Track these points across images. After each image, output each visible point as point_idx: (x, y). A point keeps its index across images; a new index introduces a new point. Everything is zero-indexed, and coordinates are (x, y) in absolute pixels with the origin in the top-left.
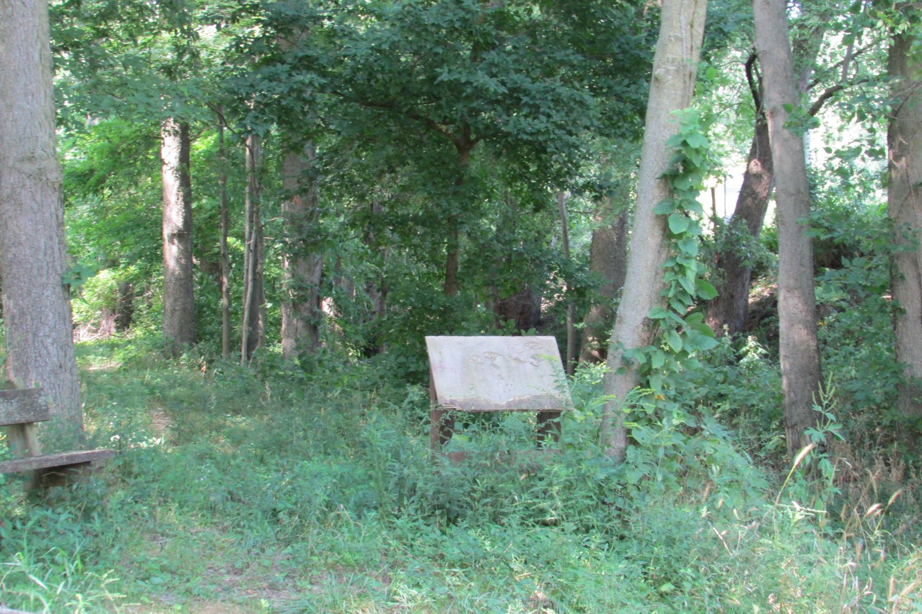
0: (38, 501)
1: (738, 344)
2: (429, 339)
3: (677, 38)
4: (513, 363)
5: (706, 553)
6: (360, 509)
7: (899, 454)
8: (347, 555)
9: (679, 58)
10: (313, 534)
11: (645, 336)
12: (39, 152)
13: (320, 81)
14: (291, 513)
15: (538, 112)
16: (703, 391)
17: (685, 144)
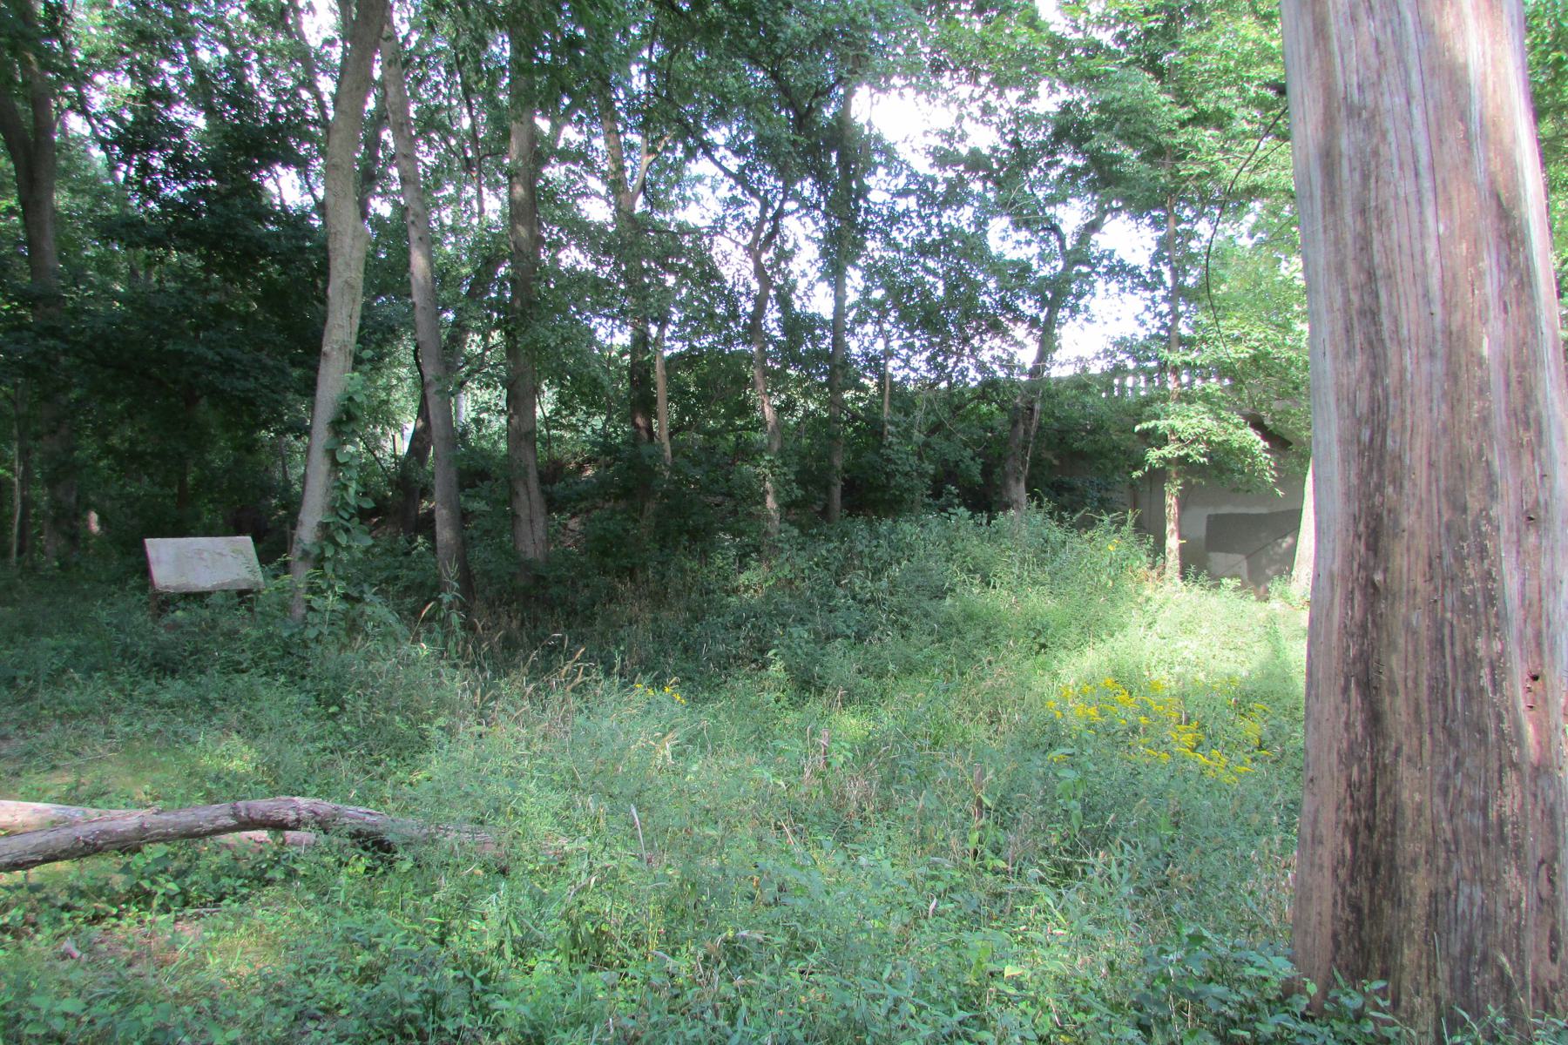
0: (175, 688)
1: (411, 541)
2: (148, 541)
5: (362, 685)
6: (89, 672)
7: (517, 611)
8: (74, 707)
10: (43, 695)
13: (61, 346)
14: (27, 679)
16: (385, 574)
17: (351, 399)
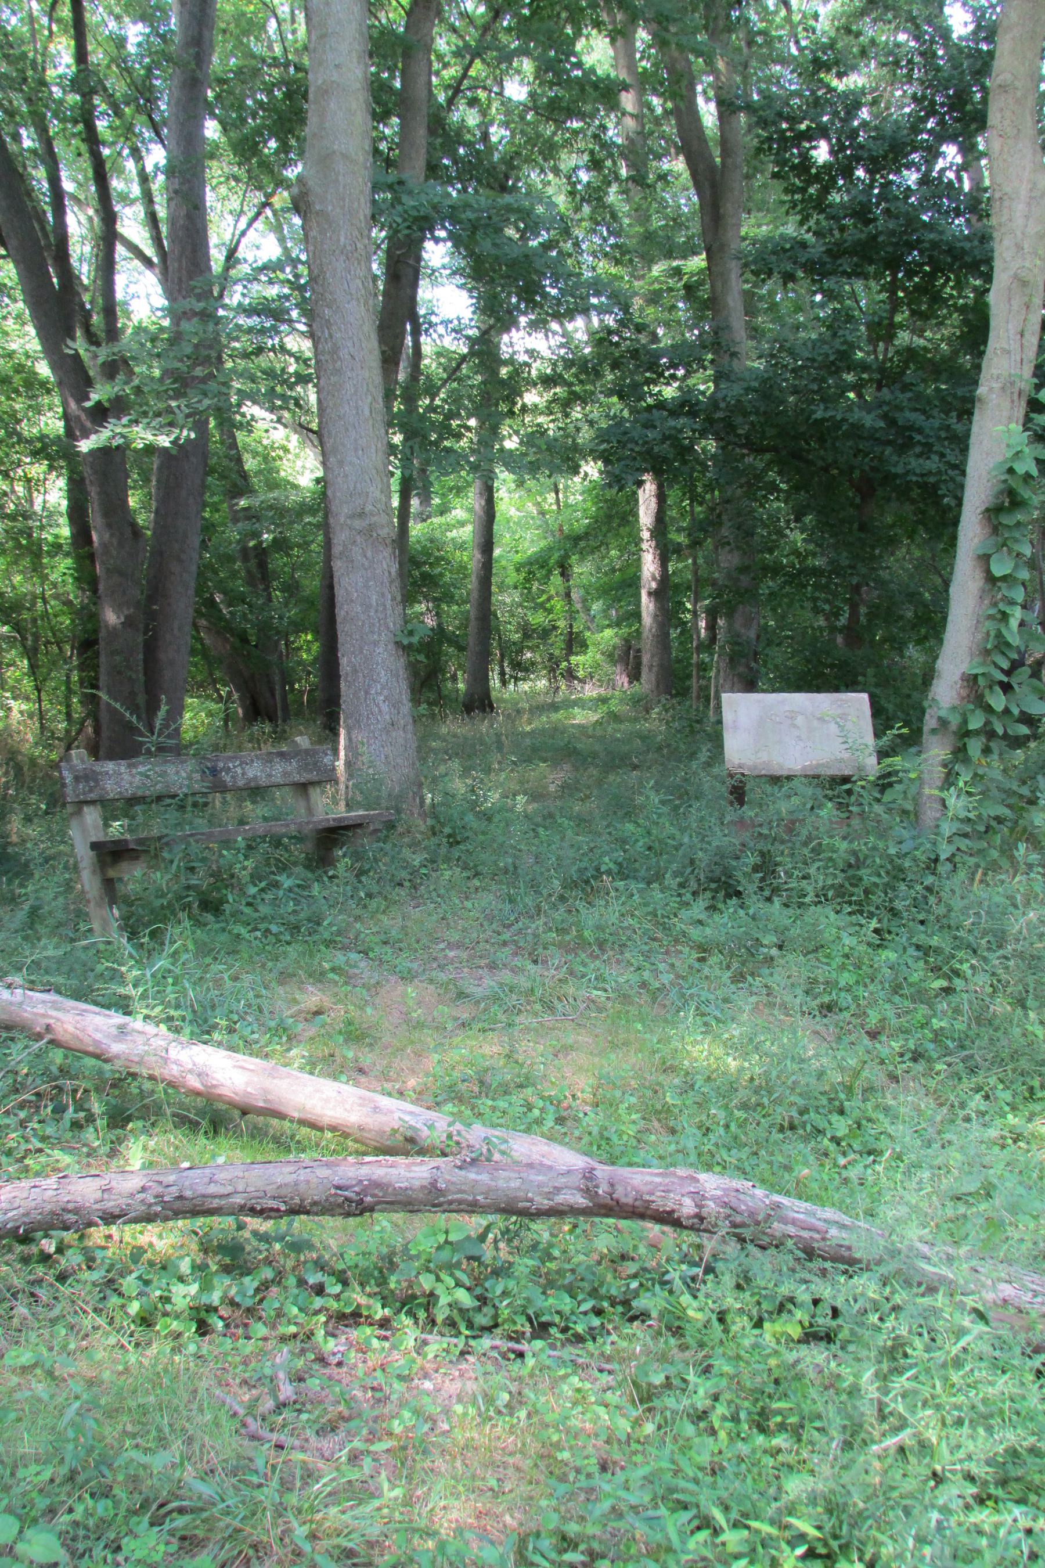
3: (1003, 350)
4: (815, 723)
9: (1005, 373)
11: (964, 693)
12: (369, 508)
15: (930, 451)
17: (1011, 471)
